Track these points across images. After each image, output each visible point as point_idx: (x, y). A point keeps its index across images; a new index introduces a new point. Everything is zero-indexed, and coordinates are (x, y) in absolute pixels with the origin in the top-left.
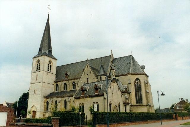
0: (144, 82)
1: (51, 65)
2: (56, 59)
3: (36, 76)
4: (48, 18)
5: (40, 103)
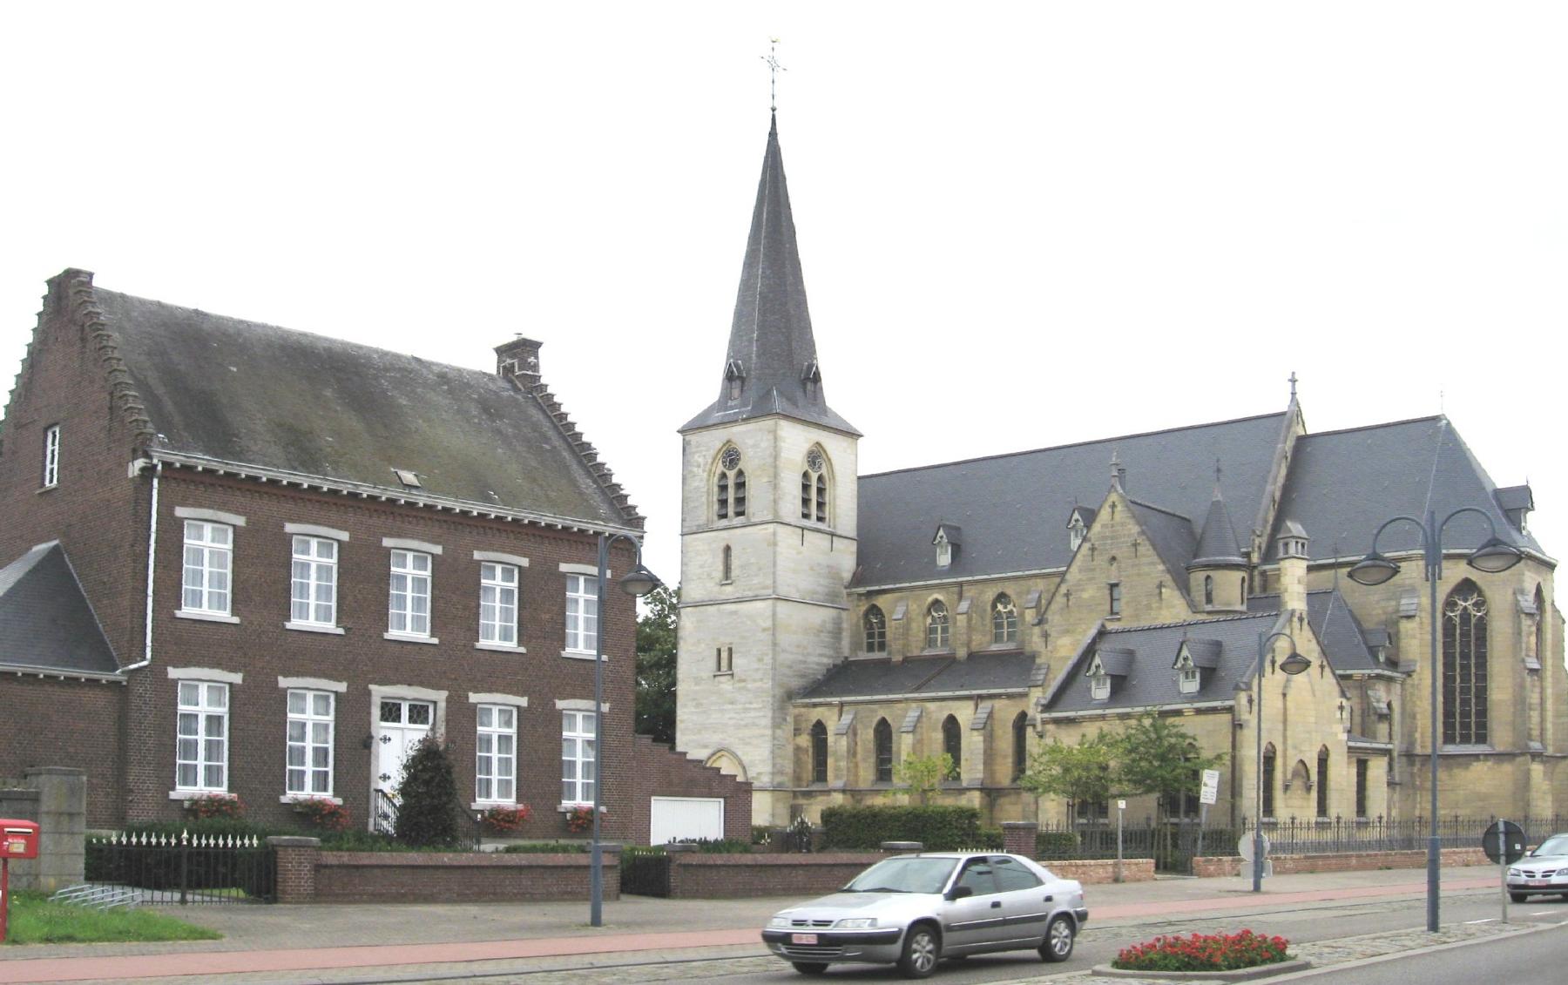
0: (1517, 603)
1: (820, 479)
2: (853, 435)
3: (721, 556)
4: (773, 134)
5: (769, 732)
